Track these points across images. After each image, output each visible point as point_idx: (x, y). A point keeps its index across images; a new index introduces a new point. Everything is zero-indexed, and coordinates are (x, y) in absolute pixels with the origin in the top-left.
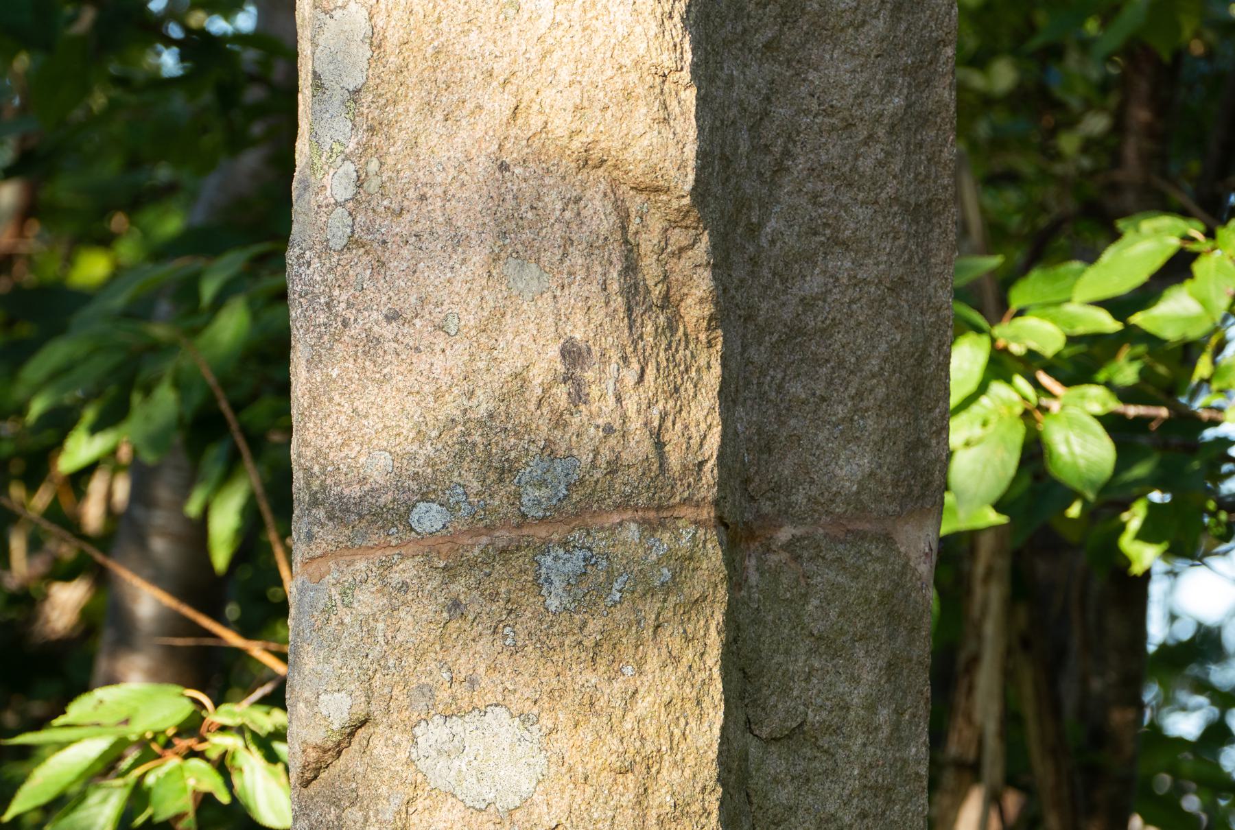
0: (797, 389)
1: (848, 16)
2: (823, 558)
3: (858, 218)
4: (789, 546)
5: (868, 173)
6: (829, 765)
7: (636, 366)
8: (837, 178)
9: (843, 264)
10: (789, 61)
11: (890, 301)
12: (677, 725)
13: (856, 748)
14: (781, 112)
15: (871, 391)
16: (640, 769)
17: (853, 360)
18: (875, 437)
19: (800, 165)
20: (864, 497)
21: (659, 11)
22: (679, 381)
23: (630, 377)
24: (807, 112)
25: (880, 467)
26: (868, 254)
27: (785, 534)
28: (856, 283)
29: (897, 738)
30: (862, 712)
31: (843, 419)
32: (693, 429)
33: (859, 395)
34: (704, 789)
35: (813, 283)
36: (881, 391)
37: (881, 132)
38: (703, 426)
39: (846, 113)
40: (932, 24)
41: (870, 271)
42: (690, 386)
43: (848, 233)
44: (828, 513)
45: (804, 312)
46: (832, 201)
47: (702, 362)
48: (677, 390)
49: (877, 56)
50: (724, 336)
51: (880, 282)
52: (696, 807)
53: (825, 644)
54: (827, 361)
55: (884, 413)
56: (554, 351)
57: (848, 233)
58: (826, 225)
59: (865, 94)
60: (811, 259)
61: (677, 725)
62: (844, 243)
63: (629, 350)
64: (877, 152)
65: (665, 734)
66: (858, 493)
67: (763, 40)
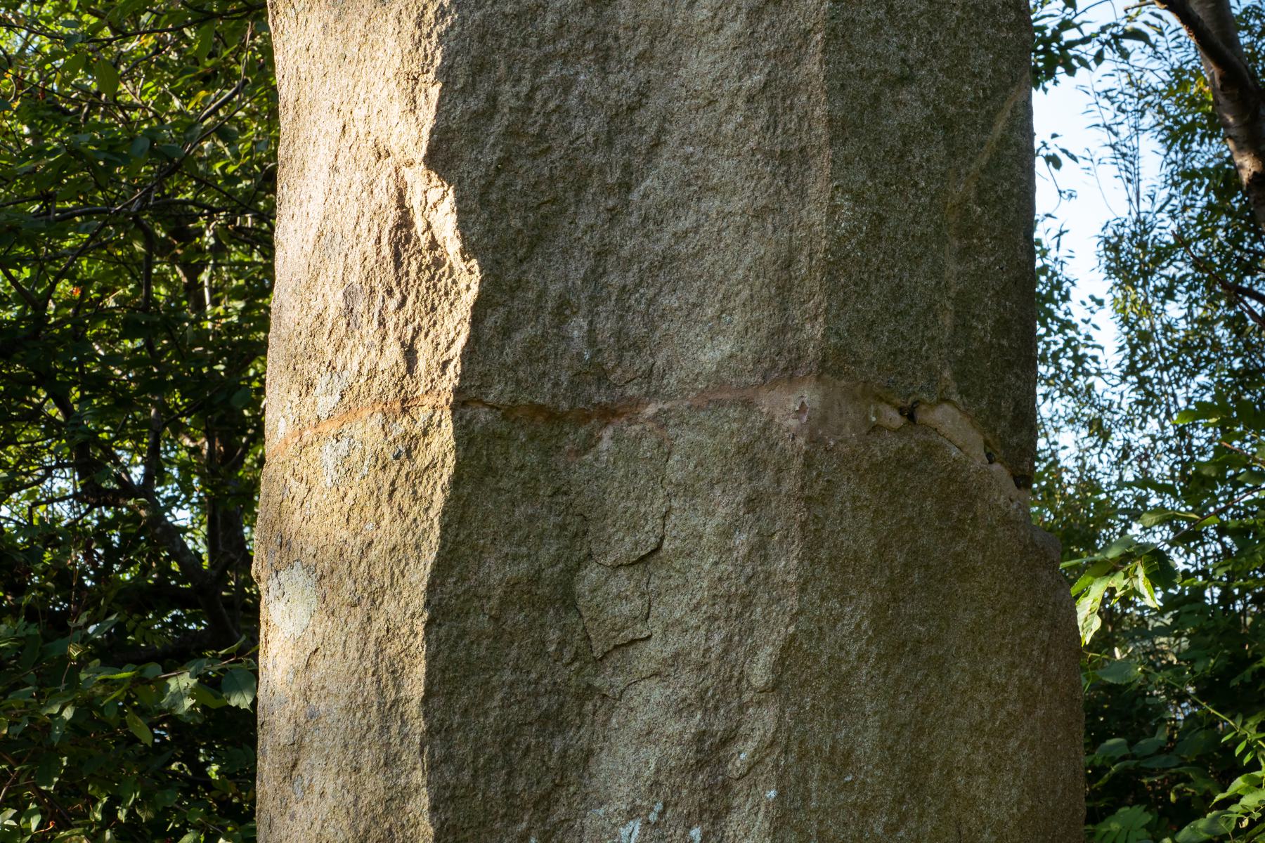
0: (670, 301)
1: (708, 24)
2: (687, 423)
3: (724, 168)
4: (654, 418)
5: (730, 133)
6: (681, 581)
7: (398, 296)
8: (704, 142)
9: (712, 204)
10: (662, 65)
11: (754, 225)
12: (398, 566)
13: (707, 567)
14: (656, 102)
15: (737, 294)
16: (366, 603)
17: (722, 273)
18: (739, 328)
19: (673, 139)
20: (724, 375)
21: (418, 33)
22: (437, 302)
23: (392, 304)
24: (678, 99)
25: (742, 350)
26: (734, 193)
27: (651, 410)
28: (723, 215)
29: (760, 549)
30: (714, 538)
31: (712, 318)
32: (442, 337)
33: (726, 297)
34: (413, 615)
35: (687, 222)
36: (745, 294)
37: (740, 102)
38: (452, 334)
39: (707, 94)
40: (801, 19)
41: (737, 204)
42: (446, 306)
43: (715, 181)
44: (694, 390)
45: (676, 243)
46: (701, 159)
47: (462, 286)
48: (434, 309)
49: (734, 49)
50: (480, 265)
51: (744, 212)
52: (405, 630)
53: (687, 489)
54: (701, 276)
55: (748, 309)
56: (340, 295)
57: (715, 181)
58: (697, 177)
59: (723, 77)
60: (685, 205)
61: (398, 566)
62: (713, 189)
63: (394, 284)
64: (738, 118)
65: (387, 574)
66: (717, 372)
67: (635, 53)
